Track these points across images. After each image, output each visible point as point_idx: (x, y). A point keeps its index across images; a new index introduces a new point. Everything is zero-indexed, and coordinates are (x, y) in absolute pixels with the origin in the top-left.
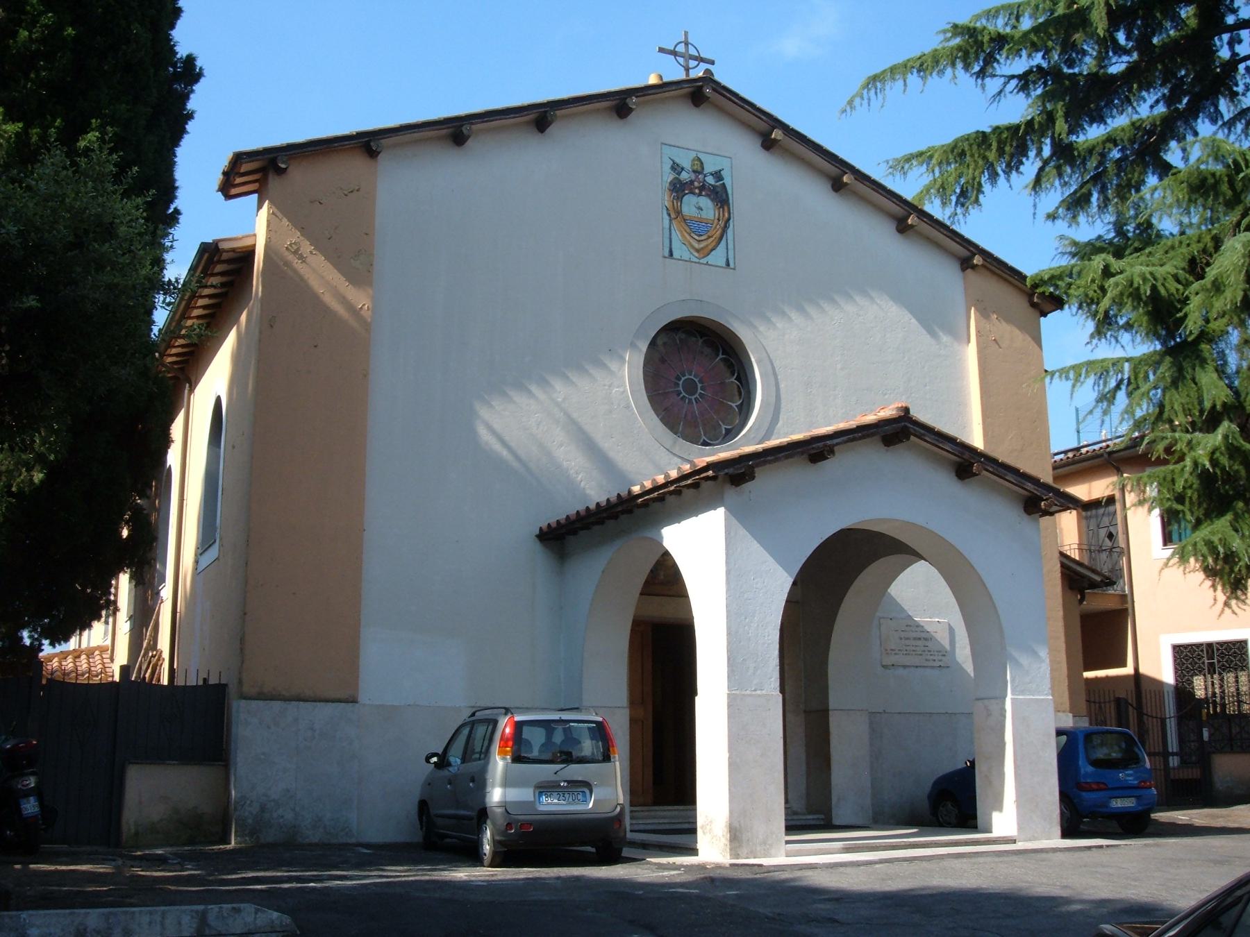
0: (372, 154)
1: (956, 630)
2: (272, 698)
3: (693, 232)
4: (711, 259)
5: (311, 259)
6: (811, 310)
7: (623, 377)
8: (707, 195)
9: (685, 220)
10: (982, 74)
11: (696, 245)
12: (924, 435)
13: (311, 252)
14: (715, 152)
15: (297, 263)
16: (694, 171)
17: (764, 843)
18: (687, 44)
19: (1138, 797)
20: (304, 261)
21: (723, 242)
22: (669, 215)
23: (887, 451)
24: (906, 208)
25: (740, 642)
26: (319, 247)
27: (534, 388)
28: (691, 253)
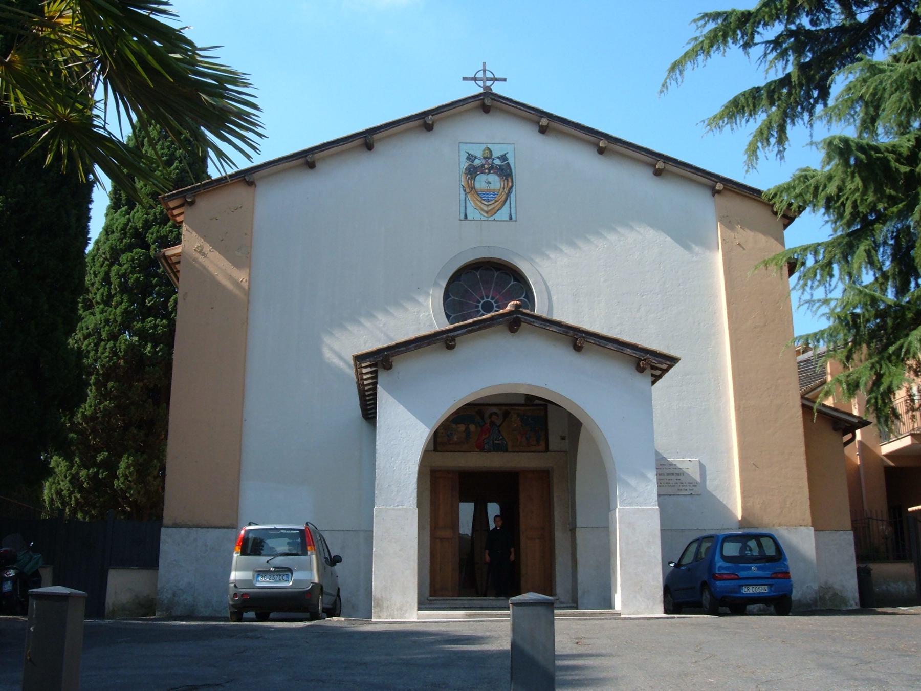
0: (251, 184)
2: (181, 526)
3: (484, 200)
4: (498, 216)
5: (210, 255)
6: (580, 243)
7: (428, 305)
8: (495, 173)
9: (477, 192)
10: (747, 46)
11: (486, 209)
12: (534, 322)
13: (210, 251)
14: (502, 142)
15: (201, 259)
16: (484, 158)
17: (401, 609)
18: (484, 71)
19: (770, 585)
20: (205, 257)
21: (508, 202)
22: (465, 191)
23: (513, 336)
24: (654, 157)
25: (387, 473)
26: (215, 247)
27: (363, 320)
28: (481, 214)
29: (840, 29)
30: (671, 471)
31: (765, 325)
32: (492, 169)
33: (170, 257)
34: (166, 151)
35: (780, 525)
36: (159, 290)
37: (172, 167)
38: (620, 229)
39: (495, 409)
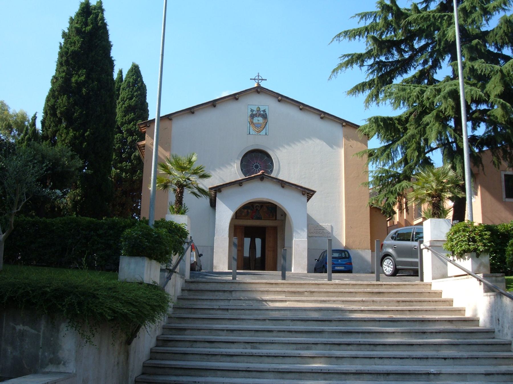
0: (171, 119)
1: (334, 227)
4: (261, 133)
11: (257, 130)
18: (258, 76)
21: (265, 128)
29: (398, 61)
30: (320, 228)
31: (358, 176)
32: (260, 115)
33: (140, 145)
34: (130, 93)
35: (359, 249)
36: (128, 151)
37: (133, 100)
38: (307, 140)
39: (257, 204)
